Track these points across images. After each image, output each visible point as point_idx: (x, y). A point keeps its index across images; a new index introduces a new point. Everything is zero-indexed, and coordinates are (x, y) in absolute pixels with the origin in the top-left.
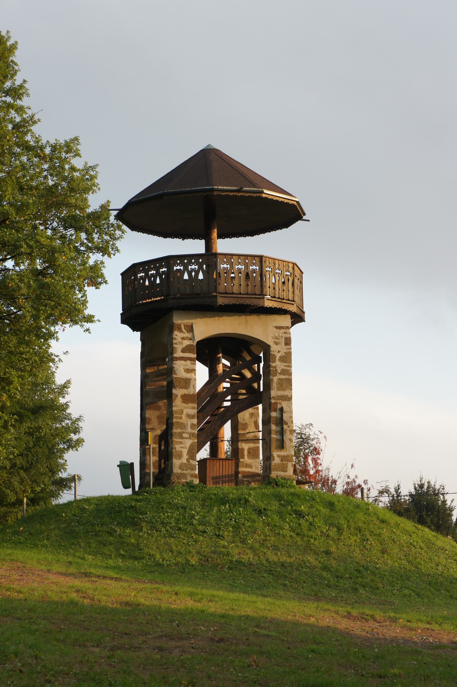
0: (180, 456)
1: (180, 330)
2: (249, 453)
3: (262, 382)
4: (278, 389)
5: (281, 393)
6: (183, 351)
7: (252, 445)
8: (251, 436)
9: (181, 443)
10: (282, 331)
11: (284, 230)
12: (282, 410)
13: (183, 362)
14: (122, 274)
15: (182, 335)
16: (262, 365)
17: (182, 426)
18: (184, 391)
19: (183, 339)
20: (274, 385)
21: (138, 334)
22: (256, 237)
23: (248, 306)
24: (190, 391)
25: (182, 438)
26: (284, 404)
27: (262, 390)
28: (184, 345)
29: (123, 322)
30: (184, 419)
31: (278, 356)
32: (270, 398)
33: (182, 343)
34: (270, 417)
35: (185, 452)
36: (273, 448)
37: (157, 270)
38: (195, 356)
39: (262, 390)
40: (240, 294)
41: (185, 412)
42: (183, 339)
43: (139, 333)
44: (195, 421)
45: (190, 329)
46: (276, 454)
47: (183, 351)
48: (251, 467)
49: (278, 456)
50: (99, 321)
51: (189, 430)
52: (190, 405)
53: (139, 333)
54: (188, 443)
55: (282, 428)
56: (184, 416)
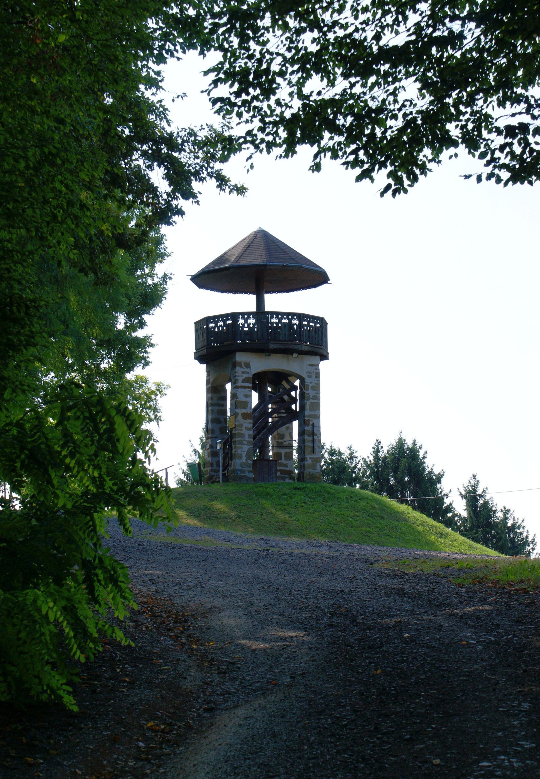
0: (241, 457)
1: (241, 367)
2: (285, 456)
3: (298, 404)
4: (310, 410)
5: (312, 413)
6: (243, 381)
7: (287, 450)
8: (286, 443)
9: (242, 448)
10: (314, 367)
11: (313, 289)
12: (313, 425)
13: (243, 390)
14: (196, 323)
15: (243, 370)
16: (298, 391)
17: (242, 436)
18: (244, 411)
19: (243, 373)
20: (307, 407)
21: (204, 366)
22: (291, 293)
23: (291, 349)
24: (249, 411)
25: (243, 444)
26: (315, 421)
27: (298, 410)
28: (243, 378)
29: (195, 358)
30: (244, 431)
31: (310, 385)
32: (304, 416)
33: (242, 376)
34: (304, 430)
35: (244, 455)
36: (306, 453)
37: (225, 322)
38: (251, 385)
39: (298, 410)
40: (285, 341)
41: (245, 425)
42: (243, 373)
43: (205, 365)
44: (251, 432)
45: (248, 365)
46: (308, 457)
47: (243, 381)
48: (287, 466)
49: (310, 458)
50: (474, 476)
51: (247, 438)
52: (248, 421)
53: (205, 365)
54: (246, 448)
55: (313, 438)
56: (243, 428)
